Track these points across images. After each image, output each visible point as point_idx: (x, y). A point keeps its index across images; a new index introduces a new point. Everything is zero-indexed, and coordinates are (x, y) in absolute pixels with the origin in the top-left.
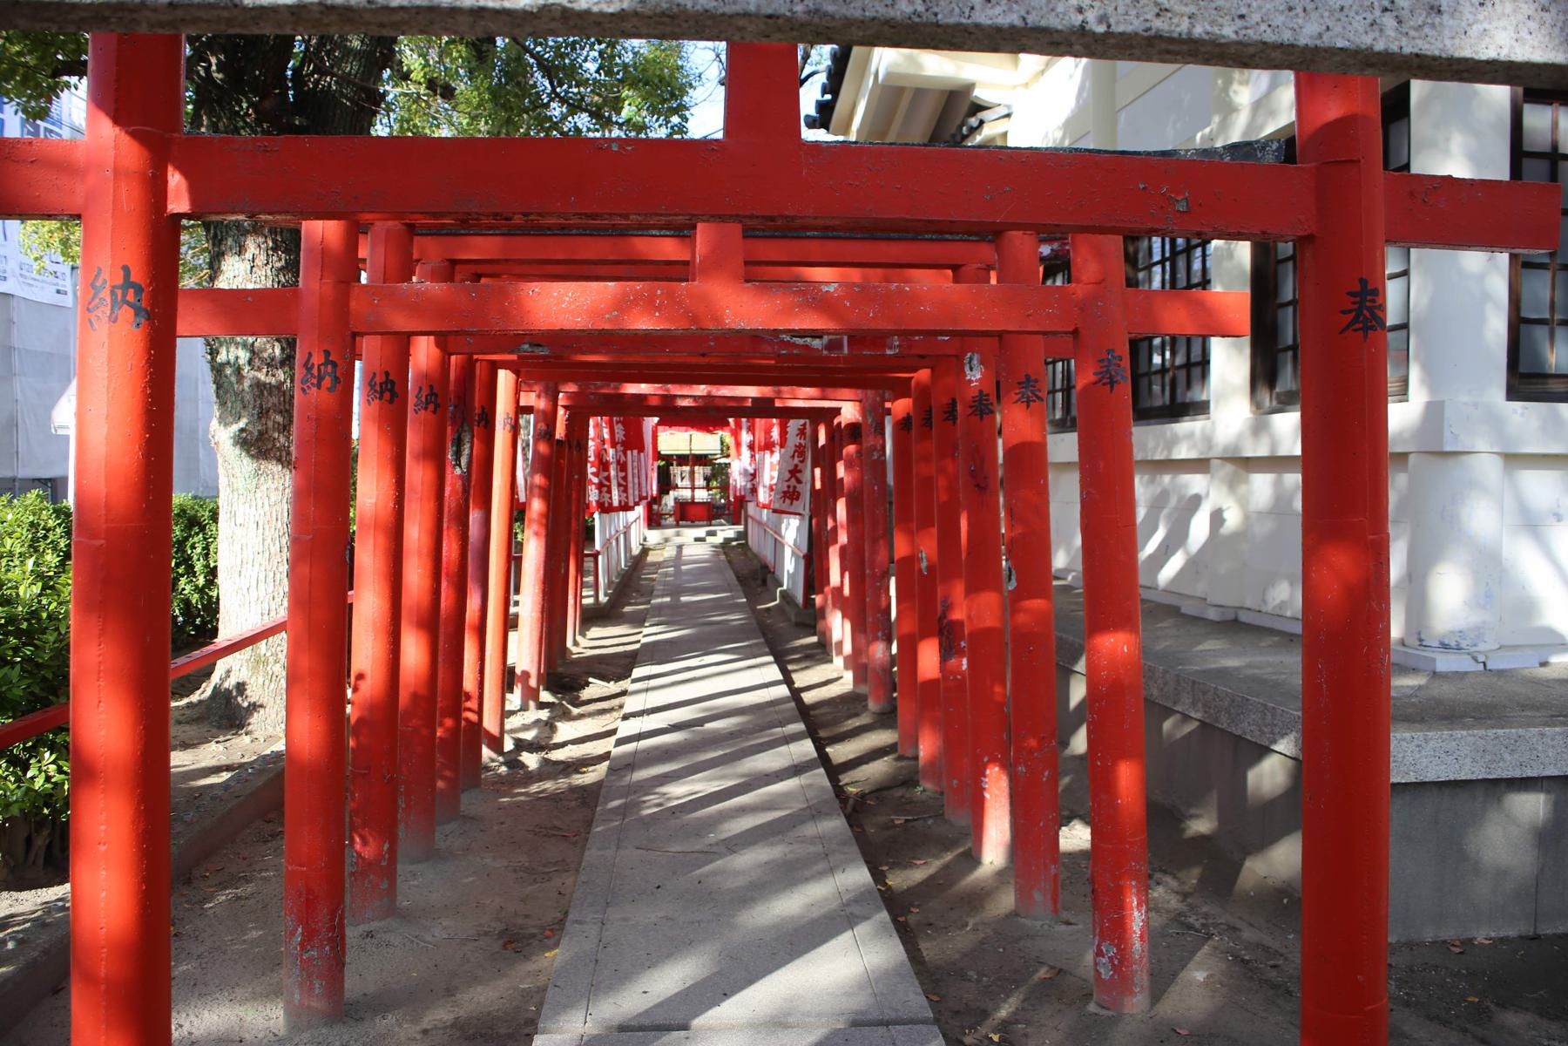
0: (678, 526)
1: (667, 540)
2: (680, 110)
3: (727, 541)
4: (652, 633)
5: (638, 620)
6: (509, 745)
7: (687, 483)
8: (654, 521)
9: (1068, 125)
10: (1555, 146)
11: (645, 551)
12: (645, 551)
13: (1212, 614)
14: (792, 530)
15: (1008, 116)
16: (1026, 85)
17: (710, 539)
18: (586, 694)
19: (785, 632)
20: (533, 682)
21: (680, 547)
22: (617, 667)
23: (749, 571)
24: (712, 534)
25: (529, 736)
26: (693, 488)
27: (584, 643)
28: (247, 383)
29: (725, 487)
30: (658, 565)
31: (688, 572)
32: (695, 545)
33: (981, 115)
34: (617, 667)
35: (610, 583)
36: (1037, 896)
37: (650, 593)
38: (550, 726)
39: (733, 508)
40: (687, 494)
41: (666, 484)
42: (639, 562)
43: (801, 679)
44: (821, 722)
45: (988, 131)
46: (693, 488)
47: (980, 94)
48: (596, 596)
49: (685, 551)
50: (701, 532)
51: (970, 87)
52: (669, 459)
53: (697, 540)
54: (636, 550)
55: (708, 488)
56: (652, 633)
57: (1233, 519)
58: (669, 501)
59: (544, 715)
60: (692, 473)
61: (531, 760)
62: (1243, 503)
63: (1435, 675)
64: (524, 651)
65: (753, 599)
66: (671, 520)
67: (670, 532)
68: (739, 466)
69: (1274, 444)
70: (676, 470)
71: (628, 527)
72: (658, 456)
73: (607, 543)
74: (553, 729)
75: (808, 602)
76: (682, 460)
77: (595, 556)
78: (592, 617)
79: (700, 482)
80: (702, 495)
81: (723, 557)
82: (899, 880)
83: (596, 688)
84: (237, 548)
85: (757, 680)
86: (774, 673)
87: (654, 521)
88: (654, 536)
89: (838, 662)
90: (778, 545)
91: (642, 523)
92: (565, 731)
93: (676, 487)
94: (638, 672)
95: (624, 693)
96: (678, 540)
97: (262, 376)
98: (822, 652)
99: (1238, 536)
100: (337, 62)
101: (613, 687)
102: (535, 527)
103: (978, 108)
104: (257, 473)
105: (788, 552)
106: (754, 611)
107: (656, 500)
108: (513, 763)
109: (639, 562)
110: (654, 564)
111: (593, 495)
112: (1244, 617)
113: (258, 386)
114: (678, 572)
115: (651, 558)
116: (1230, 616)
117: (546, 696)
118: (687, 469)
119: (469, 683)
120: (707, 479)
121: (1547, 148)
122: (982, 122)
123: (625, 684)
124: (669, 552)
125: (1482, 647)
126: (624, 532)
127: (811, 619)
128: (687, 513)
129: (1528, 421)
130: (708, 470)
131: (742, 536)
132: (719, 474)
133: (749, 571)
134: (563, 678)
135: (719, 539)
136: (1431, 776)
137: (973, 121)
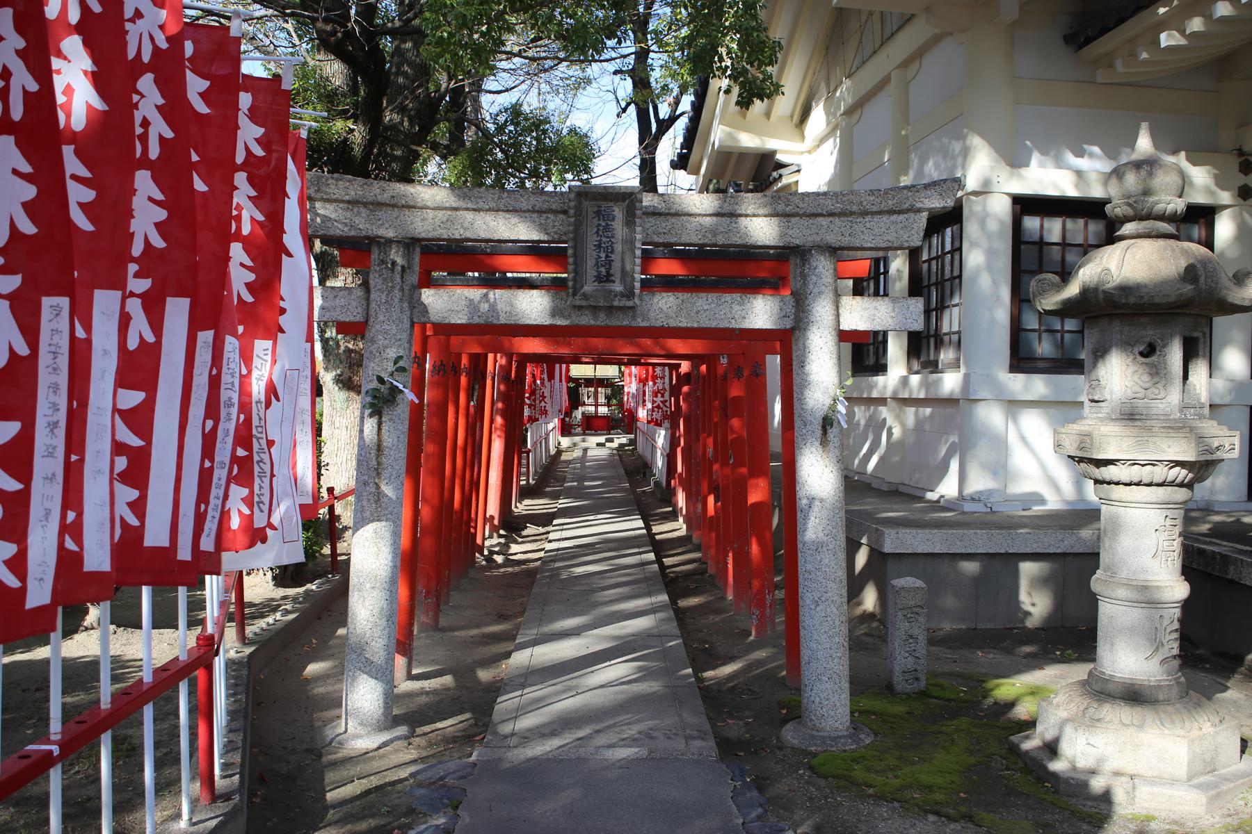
0: (584, 434)
1: (575, 445)
2: (588, 170)
3: (622, 446)
4: (563, 503)
5: (555, 496)
6: (486, 553)
7: (591, 400)
8: (566, 430)
9: (830, 183)
10: (1041, 237)
11: (559, 452)
12: (559, 452)
13: (885, 488)
14: (661, 438)
15: (798, 171)
16: (809, 152)
17: (608, 444)
18: (525, 533)
19: (651, 504)
20: (496, 522)
21: (585, 450)
22: (545, 520)
23: (632, 466)
24: (611, 440)
25: (497, 549)
26: (597, 405)
27: (521, 507)
28: (342, 348)
29: (621, 405)
30: (569, 462)
31: (590, 467)
32: (597, 447)
33: (782, 171)
34: (545, 520)
35: (536, 472)
36: (742, 605)
37: (564, 480)
38: (507, 546)
39: (626, 422)
40: (592, 409)
41: (575, 401)
42: (555, 458)
43: (655, 529)
44: (660, 548)
45: (785, 181)
46: (597, 405)
47: (780, 157)
48: (528, 480)
49: (590, 453)
50: (602, 439)
51: (773, 153)
52: (576, 380)
53: (598, 445)
54: (553, 452)
55: (608, 405)
56: (563, 503)
57: (897, 432)
58: (578, 414)
59: (502, 540)
60: (596, 393)
61: (499, 559)
62: (903, 425)
63: (964, 513)
64: (493, 509)
65: (634, 484)
66: (579, 430)
67: (577, 439)
68: (631, 387)
69: (910, 393)
70: (584, 391)
71: (547, 434)
72: (569, 379)
73: (534, 444)
74: (509, 547)
75: (668, 483)
76: (589, 382)
77: (528, 452)
78: (526, 493)
79: (602, 400)
80: (603, 410)
81: (617, 458)
82: (683, 603)
83: (531, 530)
84: (335, 441)
85: (633, 525)
86: (640, 523)
87: (566, 430)
88: (565, 442)
89: (681, 519)
90: (654, 448)
91: (557, 432)
92: (514, 548)
93: (584, 404)
94: (555, 522)
95: (548, 533)
96: (584, 445)
97: (350, 346)
98: (673, 516)
99: (901, 442)
100: (388, 164)
101: (541, 530)
102: (499, 433)
103: (782, 166)
104: (348, 400)
105: (659, 452)
106: (634, 492)
107: (568, 413)
108: (489, 559)
109: (555, 458)
110: (565, 461)
111: (527, 412)
112: (901, 489)
113: (348, 350)
114: (583, 467)
115: (564, 457)
116: (893, 488)
117: (502, 532)
118: (592, 389)
119: (473, 515)
120: (608, 398)
121: (1036, 238)
122: (781, 176)
123: (551, 528)
124: (577, 453)
125: (992, 500)
126: (548, 435)
127: (667, 497)
128: (591, 425)
129: (1019, 384)
130: (609, 391)
131: (632, 442)
132: (615, 390)
133: (632, 466)
134: (512, 525)
135: (615, 445)
136: (920, 551)
137: (775, 174)
